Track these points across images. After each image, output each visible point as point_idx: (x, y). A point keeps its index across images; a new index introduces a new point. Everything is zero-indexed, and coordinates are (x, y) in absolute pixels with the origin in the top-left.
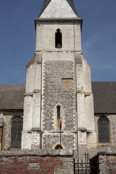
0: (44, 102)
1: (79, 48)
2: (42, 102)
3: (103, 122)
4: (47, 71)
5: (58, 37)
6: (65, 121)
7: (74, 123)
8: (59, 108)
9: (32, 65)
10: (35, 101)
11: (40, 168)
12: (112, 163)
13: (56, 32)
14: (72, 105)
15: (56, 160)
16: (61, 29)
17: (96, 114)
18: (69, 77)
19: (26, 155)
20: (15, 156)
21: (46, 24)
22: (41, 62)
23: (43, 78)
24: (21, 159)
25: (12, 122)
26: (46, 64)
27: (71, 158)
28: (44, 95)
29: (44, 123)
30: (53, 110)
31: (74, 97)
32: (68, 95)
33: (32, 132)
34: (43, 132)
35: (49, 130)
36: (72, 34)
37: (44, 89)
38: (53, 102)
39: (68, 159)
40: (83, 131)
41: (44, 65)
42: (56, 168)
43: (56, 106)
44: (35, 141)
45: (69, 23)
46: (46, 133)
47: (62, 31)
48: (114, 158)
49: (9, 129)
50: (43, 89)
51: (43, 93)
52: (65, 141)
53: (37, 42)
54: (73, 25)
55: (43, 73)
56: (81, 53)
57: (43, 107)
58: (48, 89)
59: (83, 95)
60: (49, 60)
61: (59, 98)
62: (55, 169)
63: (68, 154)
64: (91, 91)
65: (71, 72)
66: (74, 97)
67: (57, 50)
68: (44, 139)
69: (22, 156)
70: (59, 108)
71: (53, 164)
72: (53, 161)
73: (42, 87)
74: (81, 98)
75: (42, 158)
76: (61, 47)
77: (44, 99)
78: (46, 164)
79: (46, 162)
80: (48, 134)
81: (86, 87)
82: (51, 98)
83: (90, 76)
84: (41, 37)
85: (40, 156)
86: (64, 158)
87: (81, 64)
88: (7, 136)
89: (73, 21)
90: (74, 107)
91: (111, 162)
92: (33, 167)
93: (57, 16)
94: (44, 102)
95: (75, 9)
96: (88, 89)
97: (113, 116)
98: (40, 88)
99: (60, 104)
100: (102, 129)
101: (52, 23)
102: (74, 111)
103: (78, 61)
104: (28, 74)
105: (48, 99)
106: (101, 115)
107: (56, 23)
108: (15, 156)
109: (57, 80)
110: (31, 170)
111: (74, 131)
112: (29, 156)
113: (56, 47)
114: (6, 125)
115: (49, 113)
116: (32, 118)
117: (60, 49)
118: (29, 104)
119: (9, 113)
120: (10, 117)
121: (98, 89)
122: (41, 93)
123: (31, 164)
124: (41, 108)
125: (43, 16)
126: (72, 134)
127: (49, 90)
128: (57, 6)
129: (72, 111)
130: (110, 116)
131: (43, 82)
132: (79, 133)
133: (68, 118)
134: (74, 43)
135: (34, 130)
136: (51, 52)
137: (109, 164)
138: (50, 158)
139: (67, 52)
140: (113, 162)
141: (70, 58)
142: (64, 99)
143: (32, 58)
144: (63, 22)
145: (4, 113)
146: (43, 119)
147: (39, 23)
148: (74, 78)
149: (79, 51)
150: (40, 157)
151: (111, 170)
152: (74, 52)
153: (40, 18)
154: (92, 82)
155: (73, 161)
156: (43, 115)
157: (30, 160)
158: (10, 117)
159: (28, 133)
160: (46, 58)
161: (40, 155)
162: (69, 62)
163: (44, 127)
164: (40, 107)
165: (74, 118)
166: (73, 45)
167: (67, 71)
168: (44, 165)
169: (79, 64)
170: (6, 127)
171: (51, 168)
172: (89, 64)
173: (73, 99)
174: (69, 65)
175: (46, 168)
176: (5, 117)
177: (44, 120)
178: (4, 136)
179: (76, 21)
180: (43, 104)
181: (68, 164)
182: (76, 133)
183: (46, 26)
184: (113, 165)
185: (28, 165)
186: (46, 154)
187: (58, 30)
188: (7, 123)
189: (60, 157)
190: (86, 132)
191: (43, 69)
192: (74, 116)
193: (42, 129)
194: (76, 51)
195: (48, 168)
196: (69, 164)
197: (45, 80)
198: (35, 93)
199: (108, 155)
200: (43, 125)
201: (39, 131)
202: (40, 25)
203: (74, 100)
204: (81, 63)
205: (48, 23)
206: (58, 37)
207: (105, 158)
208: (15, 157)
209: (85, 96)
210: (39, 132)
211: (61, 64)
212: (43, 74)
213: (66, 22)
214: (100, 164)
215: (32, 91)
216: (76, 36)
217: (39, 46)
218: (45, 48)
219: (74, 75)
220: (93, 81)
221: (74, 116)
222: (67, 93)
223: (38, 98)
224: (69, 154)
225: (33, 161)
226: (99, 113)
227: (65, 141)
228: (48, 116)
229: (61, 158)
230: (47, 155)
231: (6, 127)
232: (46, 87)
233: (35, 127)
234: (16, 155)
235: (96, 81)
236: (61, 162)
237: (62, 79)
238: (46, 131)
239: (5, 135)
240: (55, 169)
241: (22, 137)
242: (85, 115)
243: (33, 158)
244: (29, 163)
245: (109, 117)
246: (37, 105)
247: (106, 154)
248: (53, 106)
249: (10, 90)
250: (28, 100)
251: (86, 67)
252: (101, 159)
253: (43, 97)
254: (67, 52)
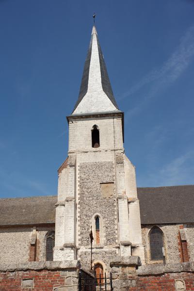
0: (79, 212)
1: (120, 145)
2: (77, 212)
3: (156, 234)
4: (82, 176)
6: (105, 234)
7: (117, 236)
8: (97, 218)
9: (64, 169)
10: (68, 211)
11: (35, 287)
12: (129, 277)
13: (93, 129)
14: (113, 215)
15: (55, 276)
16: (98, 125)
17: (143, 226)
18: (108, 181)
19: (18, 269)
20: (5, 272)
21: (80, 120)
22: (74, 164)
23: (78, 184)
24: (12, 275)
25: (48, 239)
26: (81, 167)
28: (79, 204)
29: (80, 237)
30: (90, 221)
31: (115, 204)
33: (65, 248)
34: (79, 249)
35: (87, 245)
36: (110, 129)
37: (79, 196)
38: (91, 211)
40: (126, 245)
41: (79, 168)
42: (55, 286)
43: (94, 216)
44: (68, 259)
45: (107, 117)
47: (99, 128)
48: (132, 270)
49: (43, 247)
50: (78, 196)
51: (77, 201)
52: (105, 259)
54: (112, 120)
55: (77, 178)
58: (83, 197)
59: (126, 201)
60: (85, 162)
61: (97, 207)
62: (54, 288)
63: (71, 267)
64: (137, 197)
65: (110, 175)
66: (115, 204)
67: (94, 149)
69: (14, 271)
70: (97, 218)
71: (52, 281)
72: (52, 276)
74: (123, 204)
76: (99, 146)
77: (79, 208)
78: (42, 281)
79: (43, 279)
82: (87, 208)
83: (135, 179)
84: (75, 136)
85: (36, 270)
86: (66, 272)
87: (122, 164)
88: (42, 255)
89: (112, 115)
90: (116, 217)
91: (129, 275)
92: (27, 286)
93: (94, 110)
94: (79, 212)
95: (115, 102)
96: (132, 194)
97: (167, 227)
98: (73, 196)
100: (154, 244)
101: (88, 119)
103: (120, 162)
104: (60, 180)
105: (84, 209)
106: (152, 227)
107: (92, 118)
108: (5, 272)
109: (94, 185)
110: (23, 289)
111: (116, 246)
112: (21, 271)
113: (93, 147)
114: (39, 242)
115: (85, 225)
116: (66, 231)
117: (98, 149)
119: (44, 228)
120: (45, 233)
122: (75, 201)
123: (24, 281)
124: (75, 220)
125: (77, 112)
126: (114, 249)
127: (85, 198)
129: (114, 222)
130: (165, 227)
131: (78, 188)
132: (122, 247)
133: (109, 230)
134: (114, 141)
135: (66, 246)
136: (87, 152)
137: (125, 279)
138: (47, 272)
139: (106, 151)
140: (131, 275)
141: (110, 158)
142: (104, 207)
143: (61, 158)
144: (100, 117)
145: (38, 229)
146: (78, 233)
147: (73, 120)
148: (115, 182)
149: (121, 150)
150: (34, 272)
152: (114, 150)
153: (73, 114)
155: (77, 276)
156: (78, 228)
157: (22, 277)
158: (45, 233)
159: (60, 249)
161: (35, 269)
162: (109, 162)
163: (80, 242)
165: (116, 230)
166: (113, 143)
167: (106, 174)
168: (40, 282)
169: (120, 165)
170: (40, 245)
171: (48, 286)
174: (110, 167)
175: (42, 287)
176: (38, 234)
178: (37, 255)
179: (116, 115)
180: (78, 215)
181: (70, 280)
182: (119, 248)
184: (131, 280)
186: (43, 268)
187: (95, 126)
188: (41, 241)
189: (61, 272)
190: (130, 247)
191: (77, 174)
193: (77, 245)
194: (117, 150)
195: (46, 286)
196: (72, 280)
198: (67, 201)
199: (124, 266)
200: (79, 240)
201: (73, 247)
202: (74, 122)
203: (115, 209)
204: (122, 163)
205: (82, 119)
207: (121, 271)
208: (4, 273)
209: (129, 203)
210: (74, 248)
211: (99, 166)
212: (78, 179)
213: (104, 116)
214: (113, 279)
215: (64, 200)
216: (116, 132)
218: (120, 169)
220: (139, 187)
222: (107, 200)
223: (71, 208)
224: (72, 267)
225: (27, 277)
226: (149, 225)
227: (105, 259)
228: (85, 229)
229: (61, 273)
230: (44, 269)
231: (40, 245)
232: (82, 194)
233: (68, 243)
236: (62, 278)
237: (101, 183)
238: (82, 247)
239: (39, 254)
240: (54, 288)
241: (54, 255)
242: (129, 226)
243: (27, 274)
244: (22, 280)
246: (70, 216)
249: (45, 202)
250: (59, 210)
251: (129, 168)
252: (115, 272)
253: (78, 206)
254: (106, 151)
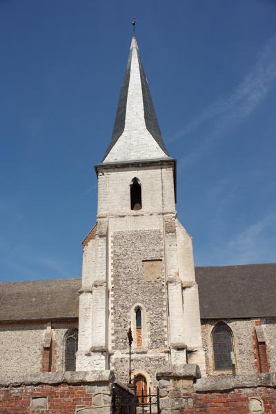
0: (113, 302)
1: (171, 206)
2: (110, 302)
3: (222, 333)
4: (117, 250)
6: (149, 333)
7: (166, 336)
8: (138, 311)
9: (91, 241)
10: (96, 300)
11: (49, 408)
12: (184, 394)
13: (132, 183)
14: (161, 306)
15: (78, 392)
16: (140, 178)
17: (204, 321)
18: (154, 257)
19: (26, 383)
20: (7, 387)
21: (114, 171)
22: (105, 234)
23: (111, 261)
24: (17, 391)
25: (68, 339)
26: (115, 237)
28: (112, 290)
29: (113, 338)
30: (128, 314)
31: (164, 291)
33: (92, 353)
34: (113, 354)
35: (123, 349)
36: (157, 184)
37: (112, 279)
38: (129, 301)
40: (180, 348)
41: (112, 239)
42: (78, 407)
43: (133, 308)
44: (96, 369)
45: (153, 167)
47: (141, 182)
48: (188, 384)
49: (61, 351)
50: (111, 279)
51: (110, 286)
52: (150, 368)
54: (160, 170)
55: (110, 253)
58: (119, 280)
59: (179, 286)
60: (120, 230)
61: (138, 295)
62: (77, 410)
63: (100, 379)
64: (194, 280)
65: (157, 248)
66: (164, 291)
67: (134, 212)
69: (19, 386)
70: (138, 311)
71: (74, 400)
72: (74, 393)
74: (175, 290)
76: (140, 207)
77: (113, 296)
78: (60, 400)
79: (61, 397)
82: (124, 296)
83: (192, 254)
84: (107, 193)
85: (51, 385)
86: (93, 387)
87: (174, 234)
88: (59, 363)
89: (159, 164)
90: (165, 309)
91: (183, 391)
92: (38, 407)
93: (133, 157)
94: (113, 302)
95: (163, 144)
96: (188, 276)
97: (238, 322)
98: (104, 278)
100: (220, 347)
101: (125, 169)
103: (170, 230)
104: (85, 256)
105: (120, 297)
106: (217, 323)
107: (131, 168)
108: (7, 387)
109: (134, 263)
111: (166, 350)
112: (30, 385)
113: (132, 209)
114: (56, 344)
115: (121, 320)
116: (94, 328)
117: (139, 212)
119: (62, 325)
120: (64, 331)
122: (107, 286)
123: (34, 400)
124: (107, 313)
125: (110, 159)
126: (162, 355)
127: (121, 282)
129: (162, 315)
130: (234, 323)
131: (111, 267)
132: (174, 352)
133: (154, 328)
134: (163, 200)
135: (94, 350)
136: (124, 216)
137: (178, 397)
138: (67, 387)
139: (151, 215)
140: (186, 391)
141: (156, 225)
142: (148, 294)
143: (87, 225)
144: (142, 166)
145: (53, 325)
146: (111, 332)
147: (103, 171)
148: (163, 259)
149: (172, 213)
150: (49, 387)
151: (183, 409)
152: (163, 214)
153: (104, 162)
155: (109, 393)
156: (111, 325)
157: (32, 394)
158: (64, 331)
159: (86, 355)
161: (50, 383)
162: (155, 231)
163: (114, 345)
165: (166, 327)
166: (161, 203)
167: (151, 247)
168: (57, 401)
169: (170, 234)
170: (57, 349)
171: (69, 407)
174: (157, 238)
175: (60, 408)
176: (54, 332)
178: (53, 363)
179: (165, 163)
180: (111, 305)
181: (100, 399)
182: (169, 352)
184: (187, 399)
186: (61, 381)
187: (135, 180)
188: (59, 342)
189: (86, 386)
190: (185, 351)
191: (110, 247)
193: (110, 349)
194: (166, 213)
195: (65, 408)
196: (103, 398)
198: (96, 286)
199: (177, 378)
200: (112, 342)
201: (103, 351)
202: (105, 173)
203: (164, 297)
204: (174, 232)
205: (117, 169)
207: (172, 385)
208: (6, 389)
209: (183, 288)
210: (105, 353)
211: (141, 236)
212: (111, 255)
213: (148, 166)
214: (161, 397)
215: (91, 284)
216: (166, 188)
218: (171, 240)
220: (197, 266)
222: (153, 284)
223: (101, 295)
224: (103, 379)
225: (38, 394)
226: (212, 319)
227: (150, 368)
228: (121, 326)
229: (87, 388)
230: (63, 383)
231: (57, 349)
232: (116, 276)
233: (97, 345)
236: (88, 395)
237: (143, 261)
238: (117, 351)
239: (55, 362)
240: (77, 410)
241: (77, 363)
242: (184, 322)
243: (38, 390)
244: (31, 399)
246: (99, 307)
249: (65, 288)
250: (84, 299)
251: (183, 239)
252: (164, 387)
253: (111, 293)
254: (151, 215)
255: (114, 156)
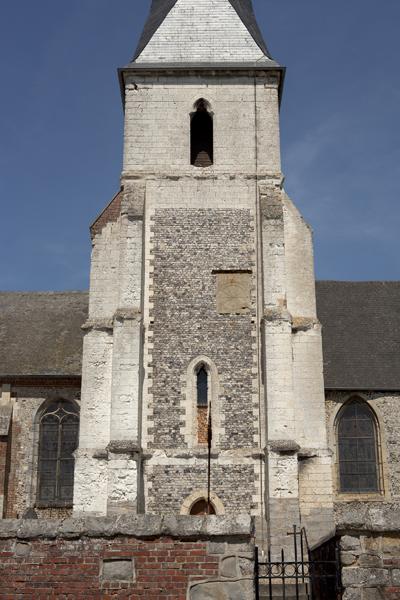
0: (151, 352)
1: (272, 164)
2: (146, 351)
3: (357, 419)
4: (162, 246)
5: (201, 128)
6: (223, 418)
7: (256, 424)
8: (202, 371)
9: (109, 224)
10: (120, 349)
11: (138, 579)
12: (385, 562)
13: (195, 110)
14: (248, 364)
15: (192, 553)
16: (211, 101)
17: (329, 394)
18: (237, 266)
19: (91, 534)
20: (53, 539)
21: (158, 83)
22: (140, 213)
23: (149, 269)
24: (72, 547)
25: (43, 421)
26: (159, 220)
27: (244, 546)
28: (151, 328)
29: (151, 424)
30: (182, 378)
31: (254, 334)
32: (236, 327)
33: (112, 455)
34: (150, 457)
35: (170, 447)
36: (247, 117)
37: (152, 305)
38: (184, 351)
39: (236, 548)
40: (286, 451)
41: (153, 223)
42: (193, 579)
43: (193, 365)
44: (119, 486)
45: (237, 79)
46: (159, 458)
47: (213, 108)
48: (392, 545)
49: (30, 444)
50: (148, 306)
51: (147, 320)
52: (223, 487)
53: (127, 145)
54: (252, 87)
55: (147, 252)
56: (278, 182)
57: (148, 370)
58: (164, 308)
59: (287, 327)
60: (169, 207)
61: (202, 339)
62: (190, 584)
63: (235, 532)
64: (315, 315)
65: (243, 248)
66: (254, 334)
67: (198, 171)
68: (152, 478)
69: (77, 538)
70: (202, 371)
71: (183, 565)
72: (184, 554)
73: (146, 299)
74: (278, 337)
75: (146, 545)
76: (211, 161)
77: (152, 340)
78: (157, 567)
79: (160, 560)
80: (165, 461)
81: (298, 299)
82: (174, 339)
83: (311, 263)
84: (143, 127)
85: (139, 538)
86: (221, 545)
87: (279, 222)
88: (26, 468)
89: (252, 73)
90: (255, 370)
91: (384, 557)
92: (115, 577)
93: (197, 55)
94: (151, 352)
95: (258, 31)
96: (303, 306)
97: (389, 399)
98: (137, 304)
99: (207, 360)
100: (351, 446)
101: (181, 79)
102: (255, 383)
103: (269, 212)
104: (97, 255)
105: (166, 342)
106: (347, 397)
107: (193, 79)
108: (53, 539)
109: (197, 277)
110: (107, 585)
111: (255, 452)
112: (98, 537)
113: (192, 163)
114: (19, 430)
115: (168, 390)
116: (111, 406)
117: (207, 171)
118: (99, 358)
119: (33, 389)
120: (36, 402)
121: (340, 307)
122: (142, 320)
123: (107, 564)
124: (142, 373)
125: (150, 56)
126: (248, 461)
127: (168, 312)
128: (195, 20)
129: (250, 384)
130: (381, 400)
131: (149, 281)
132: (273, 458)
133: (234, 407)
134: (256, 149)
135: (116, 449)
136: (176, 179)
137: (374, 567)
138: (171, 544)
139: (232, 178)
140: (388, 557)
141: (243, 199)
142: (222, 340)
143: (111, 201)
144: (217, 76)
145: (14, 390)
146: (147, 412)
147: (136, 79)
148: (254, 269)
149: (274, 177)
150: (137, 543)
151: (383, 586)
152: (256, 178)
153: (137, 61)
154: (317, 283)
155: (251, 556)
156: (148, 398)
157: (102, 553)
158: (36, 402)
159: (95, 457)
160: (158, 199)
161: (139, 534)
162: (239, 212)
163: (151, 438)
164: (136, 369)
165: (256, 406)
166: (252, 155)
167: (231, 244)
168: (153, 567)
169: (272, 221)
170: (22, 439)
171: (174, 579)
172: (306, 219)
173: (253, 340)
174: (239, 224)
175: (159, 580)
176: (16, 405)
177: (150, 412)
178: (12, 468)
179: (263, 73)
180: (148, 358)
181: (233, 565)
182: (262, 457)
183: (157, 90)
184: (391, 570)
185: (96, 570)
186: (159, 532)
187: (201, 104)
188: (25, 426)
189: (208, 543)
190: (296, 457)
191: (147, 239)
192: (255, 399)
193: (144, 445)
194: (263, 177)
195: (167, 579)
196: (238, 565)
197: (154, 276)
198: (121, 319)
199: (373, 533)
200: (149, 432)
201: (134, 452)
202: (139, 86)
203: (254, 346)
204: (279, 217)
205: (164, 79)
206: (201, 128)
207: (363, 545)
208: (51, 542)
209: (294, 331)
210: (136, 455)
211: (211, 221)
212: (149, 257)
213: (228, 76)
214: (346, 565)
215: (111, 315)
216: (263, 124)
217: (134, 159)
218: (155, 167)
219: (254, 258)
220: (319, 279)
221: (255, 399)
222: (233, 319)
223: (132, 338)
224: (239, 532)
225: (114, 554)
226: (342, 391)
227: (223, 487)
228: (167, 401)
229: (210, 546)
230: (163, 535)
231: (22, 439)
232: (159, 300)
233: (121, 439)
234: (54, 533)
235: (330, 279)
236: (212, 559)
237: (214, 272)
238: (158, 452)
239: (18, 465)
240: (190, 584)
241: (76, 472)
242: (294, 397)
243: (115, 546)
244: (101, 562)
245: (375, 403)
246: (128, 361)
247: (364, 532)
248: (182, 367)
249: (35, 312)
250: (95, 345)
251: (295, 232)
252: (350, 548)
253: (149, 333)
254: (232, 178)
255: (150, 56)
